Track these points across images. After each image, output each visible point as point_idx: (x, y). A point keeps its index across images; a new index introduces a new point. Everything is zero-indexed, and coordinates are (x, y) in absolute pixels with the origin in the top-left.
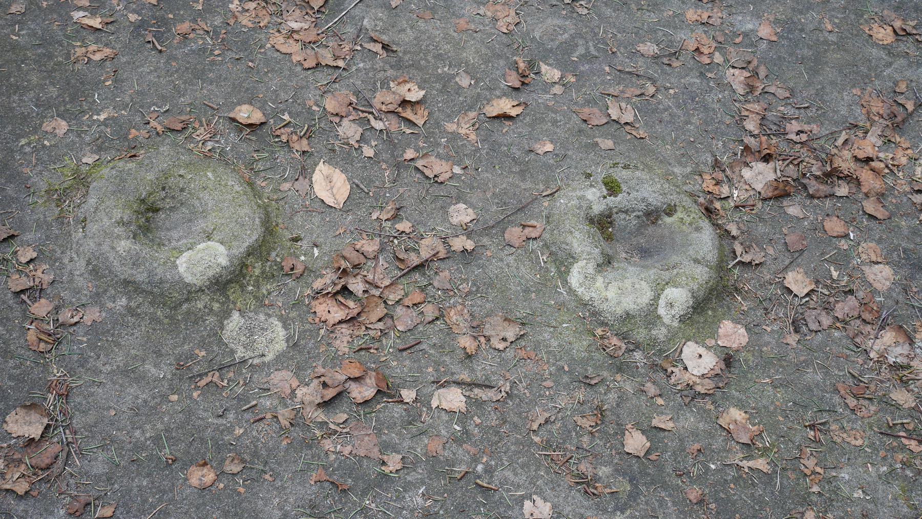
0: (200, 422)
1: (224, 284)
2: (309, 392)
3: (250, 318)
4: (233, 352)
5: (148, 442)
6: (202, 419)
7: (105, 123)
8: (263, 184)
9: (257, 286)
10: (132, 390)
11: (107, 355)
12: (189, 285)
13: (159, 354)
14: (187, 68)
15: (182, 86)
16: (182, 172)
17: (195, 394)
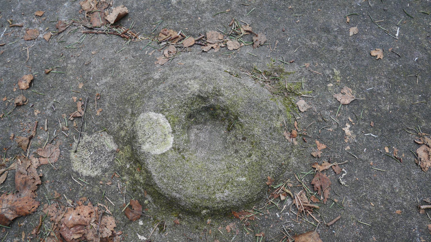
0: (58, 93)
1: (130, 141)
2: (32, 167)
3: (109, 156)
4: (90, 133)
5: (65, 64)
6: (58, 96)
7: (339, 129)
8: (228, 227)
9: (130, 173)
10: (101, 67)
11: (131, 61)
12: (139, 114)
13: (112, 87)
14: (390, 221)
15: (367, 207)
16: (254, 157)
17: (75, 98)
